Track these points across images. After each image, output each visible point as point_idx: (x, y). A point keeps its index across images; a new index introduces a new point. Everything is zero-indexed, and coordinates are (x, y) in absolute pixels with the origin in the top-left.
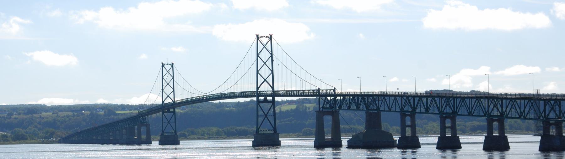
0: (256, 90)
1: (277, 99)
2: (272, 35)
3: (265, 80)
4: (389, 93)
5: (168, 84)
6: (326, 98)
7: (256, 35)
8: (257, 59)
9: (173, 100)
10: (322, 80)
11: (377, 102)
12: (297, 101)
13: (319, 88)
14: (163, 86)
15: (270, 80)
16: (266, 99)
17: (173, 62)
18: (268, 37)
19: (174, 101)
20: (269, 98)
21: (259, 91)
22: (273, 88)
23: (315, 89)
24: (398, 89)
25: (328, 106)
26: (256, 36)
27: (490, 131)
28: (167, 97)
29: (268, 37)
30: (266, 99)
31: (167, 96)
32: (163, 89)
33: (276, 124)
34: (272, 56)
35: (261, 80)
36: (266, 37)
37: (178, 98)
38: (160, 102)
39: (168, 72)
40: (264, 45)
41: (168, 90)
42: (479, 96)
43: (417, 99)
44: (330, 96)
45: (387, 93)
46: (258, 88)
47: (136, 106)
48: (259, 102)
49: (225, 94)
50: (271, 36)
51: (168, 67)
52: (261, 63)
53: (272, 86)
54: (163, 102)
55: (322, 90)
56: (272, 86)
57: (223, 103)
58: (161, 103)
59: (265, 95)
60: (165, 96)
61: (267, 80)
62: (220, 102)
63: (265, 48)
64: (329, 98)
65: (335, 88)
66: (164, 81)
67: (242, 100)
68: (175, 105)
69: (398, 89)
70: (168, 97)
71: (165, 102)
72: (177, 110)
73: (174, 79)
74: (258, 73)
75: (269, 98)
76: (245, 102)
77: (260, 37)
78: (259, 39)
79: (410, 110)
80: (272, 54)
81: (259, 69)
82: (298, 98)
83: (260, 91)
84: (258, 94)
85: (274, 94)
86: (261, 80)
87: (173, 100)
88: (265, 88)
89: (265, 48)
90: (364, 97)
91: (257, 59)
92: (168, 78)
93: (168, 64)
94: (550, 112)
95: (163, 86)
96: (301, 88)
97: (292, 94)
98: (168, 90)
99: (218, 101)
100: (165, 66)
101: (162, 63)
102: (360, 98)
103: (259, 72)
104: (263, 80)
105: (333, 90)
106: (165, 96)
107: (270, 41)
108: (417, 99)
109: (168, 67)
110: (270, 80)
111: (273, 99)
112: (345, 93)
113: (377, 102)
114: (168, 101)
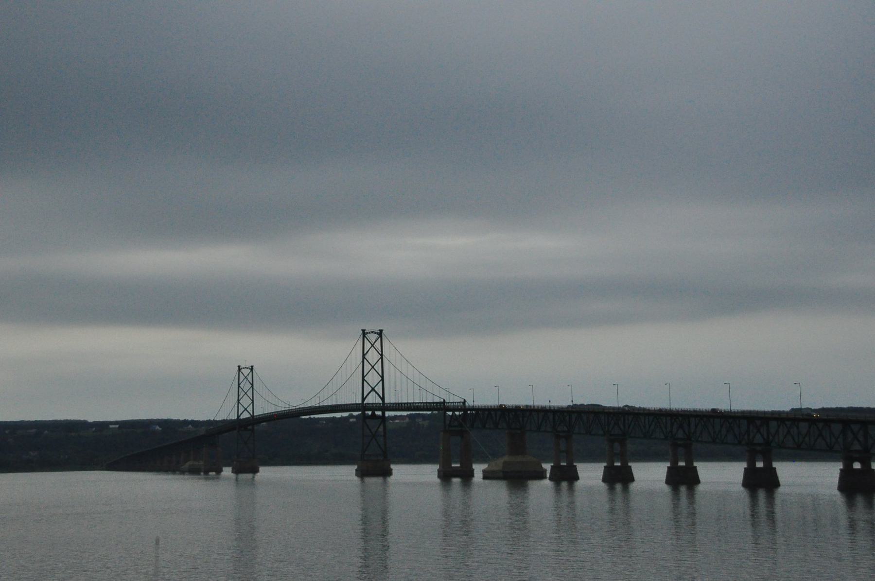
0: (360, 402)
1: (387, 414)
2: (383, 330)
3: (373, 389)
4: (485, 406)
5: (246, 393)
6: (445, 413)
7: (362, 330)
8: (363, 362)
9: (252, 414)
10: (448, 390)
11: (521, 419)
12: (408, 416)
13: (444, 400)
14: (238, 396)
15: (379, 389)
16: (373, 414)
17: (381, 329)
18: (378, 333)
19: (253, 416)
20: (379, 413)
21: (365, 403)
22: (383, 399)
23: (459, 401)
24: (550, 401)
25: (456, 423)
26: (361, 332)
27: (674, 463)
28: (244, 411)
29: (378, 333)
30: (373, 414)
31: (244, 409)
32: (238, 400)
33: (287, 418)
34: (382, 358)
35: (367, 389)
36: (248, 368)
37: (258, 412)
38: (235, 417)
39: (246, 377)
40: (372, 343)
41: (246, 401)
42: (607, 411)
43: (574, 416)
44: (459, 410)
45: (534, 406)
46: (363, 399)
47: (203, 422)
48: (364, 417)
49: (324, 407)
50: (252, 367)
51: (246, 372)
52: (367, 367)
53: (381, 396)
54: (238, 416)
55: (448, 403)
56: (381, 396)
57: (314, 418)
58: (236, 418)
59: (374, 407)
60: (241, 409)
61: (375, 389)
62: (310, 418)
63: (374, 347)
64: (457, 413)
65: (464, 400)
66: (240, 390)
67: (338, 415)
68: (254, 421)
69: (550, 401)
70: (246, 411)
71: (241, 417)
72: (256, 428)
73: (254, 387)
74: (363, 380)
75: (379, 413)
76: (342, 418)
77: (367, 333)
78: (366, 336)
79: (565, 429)
80: (382, 355)
81: (381, 382)
82: (409, 413)
83: (366, 404)
84: (363, 407)
85: (384, 407)
86: (367, 389)
87: (252, 414)
88: (373, 399)
89: (374, 347)
90: (502, 411)
91: (363, 362)
92: (246, 386)
93: (246, 368)
94: (677, 431)
95: (238, 396)
96: (395, 400)
97: (399, 408)
98: (246, 401)
99: (307, 417)
100: (242, 370)
101: (363, 331)
102: (487, 412)
103: (381, 378)
104: (371, 389)
105: (463, 402)
106: (241, 409)
107: (380, 339)
108: (574, 416)
109: (246, 372)
110: (379, 389)
111: (383, 414)
112: (494, 406)
113: (521, 419)
114: (245, 415)
